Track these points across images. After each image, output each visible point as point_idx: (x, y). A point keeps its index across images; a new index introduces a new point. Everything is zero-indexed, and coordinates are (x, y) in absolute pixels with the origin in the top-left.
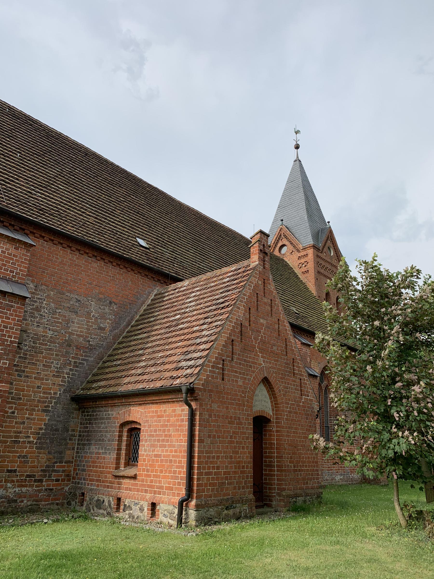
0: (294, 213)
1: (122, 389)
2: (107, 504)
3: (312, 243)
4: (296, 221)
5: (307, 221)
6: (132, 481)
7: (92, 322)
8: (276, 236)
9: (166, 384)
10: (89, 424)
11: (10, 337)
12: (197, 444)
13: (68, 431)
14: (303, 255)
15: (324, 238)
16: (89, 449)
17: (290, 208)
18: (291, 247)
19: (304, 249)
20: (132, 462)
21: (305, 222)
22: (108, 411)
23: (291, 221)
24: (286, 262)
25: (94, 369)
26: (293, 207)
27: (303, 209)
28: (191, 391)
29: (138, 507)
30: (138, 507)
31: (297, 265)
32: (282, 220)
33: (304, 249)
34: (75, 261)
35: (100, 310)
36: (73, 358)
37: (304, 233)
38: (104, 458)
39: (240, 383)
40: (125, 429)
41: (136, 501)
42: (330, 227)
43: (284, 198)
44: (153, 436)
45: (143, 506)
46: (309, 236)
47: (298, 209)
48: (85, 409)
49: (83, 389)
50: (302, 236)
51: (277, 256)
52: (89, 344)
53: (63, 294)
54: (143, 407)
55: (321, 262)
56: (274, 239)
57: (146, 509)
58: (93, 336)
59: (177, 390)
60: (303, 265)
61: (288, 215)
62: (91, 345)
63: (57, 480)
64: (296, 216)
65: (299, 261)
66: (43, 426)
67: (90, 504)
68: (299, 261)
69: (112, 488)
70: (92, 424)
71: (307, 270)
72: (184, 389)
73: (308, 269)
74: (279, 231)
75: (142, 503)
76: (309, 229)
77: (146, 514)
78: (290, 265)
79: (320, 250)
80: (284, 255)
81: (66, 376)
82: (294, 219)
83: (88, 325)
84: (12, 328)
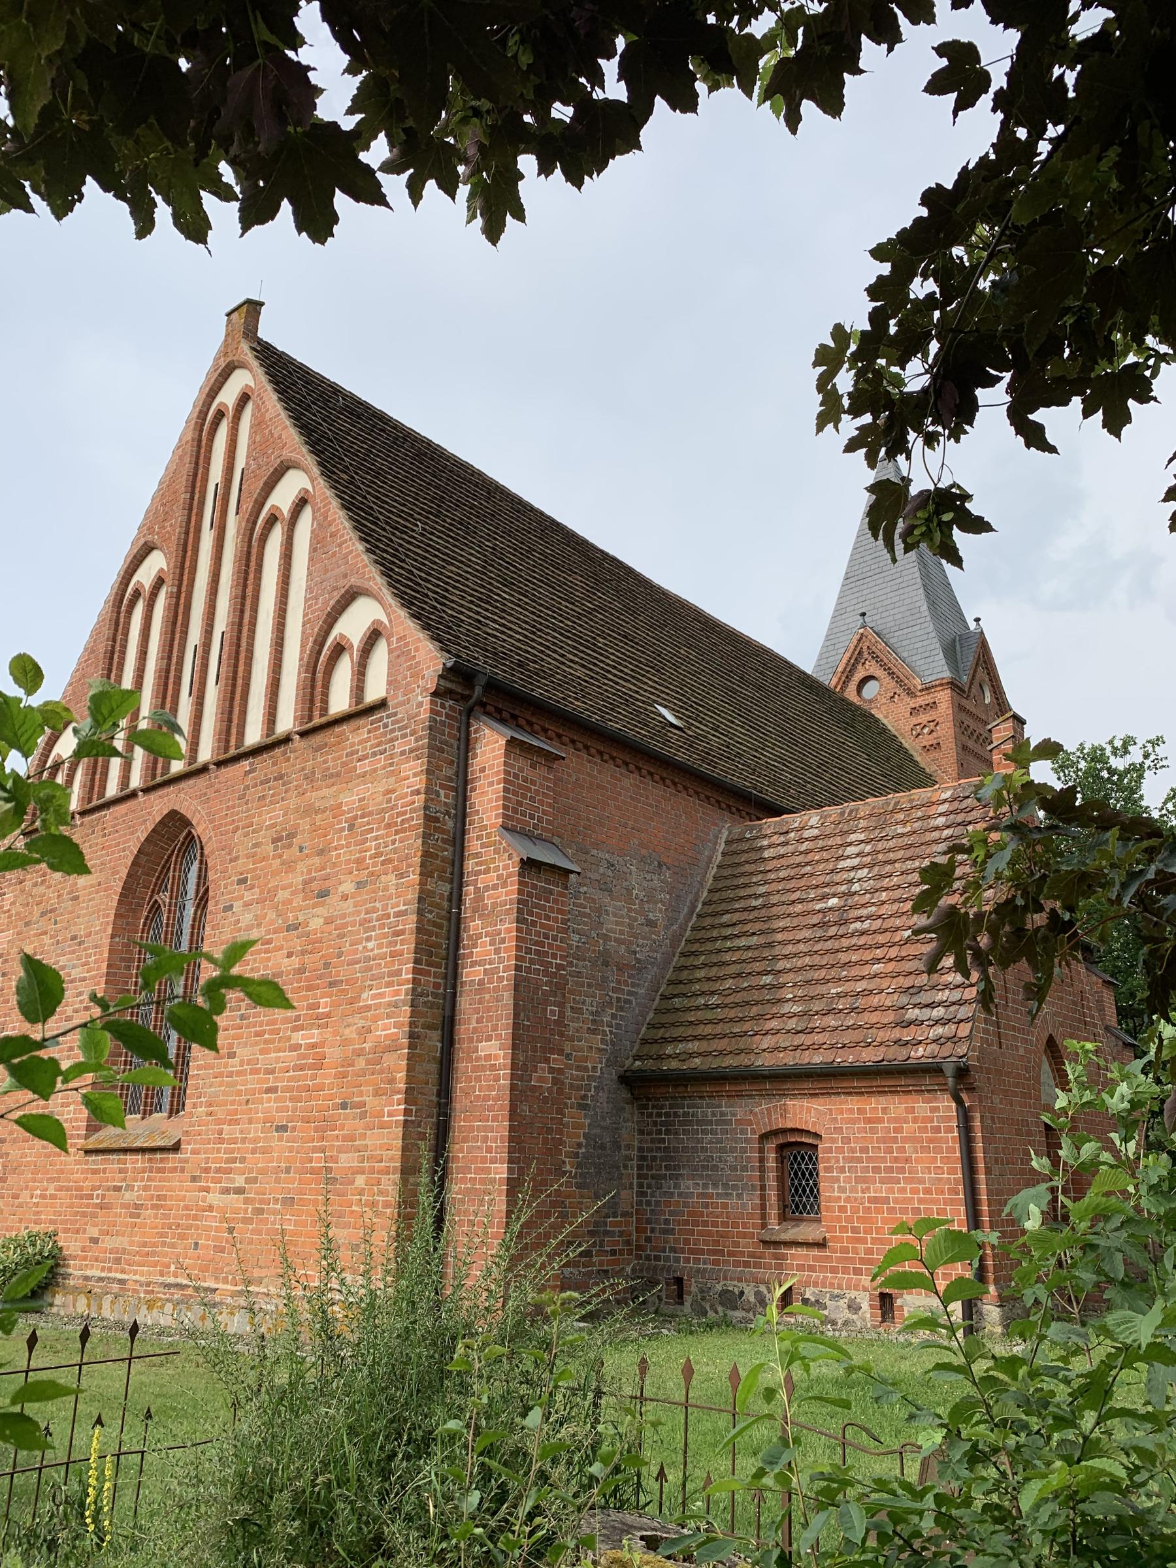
0: (889, 595)
1: (765, 1061)
2: (752, 1299)
3: (947, 674)
4: (897, 617)
5: (928, 618)
6: (815, 1252)
7: (635, 911)
8: (848, 655)
9: (891, 1057)
10: (668, 1132)
11: (554, 956)
12: (982, 1177)
13: (619, 1148)
14: (923, 703)
15: (969, 660)
16: (676, 1186)
17: (879, 582)
18: (891, 684)
19: (927, 689)
20: (793, 1212)
21: (922, 620)
22: (720, 1106)
23: (884, 615)
24: (877, 721)
25: (647, 1013)
26: (887, 579)
27: (915, 587)
28: (962, 1073)
29: (843, 1303)
30: (843, 1303)
31: (908, 728)
32: (863, 614)
33: (927, 689)
34: (595, 777)
35: (645, 884)
36: (615, 990)
37: (923, 650)
38: (725, 1206)
39: (1021, 1052)
40: (771, 1145)
41: (836, 1291)
42: (982, 633)
43: (859, 556)
44: (860, 1160)
45: (858, 1300)
46: (937, 658)
47: (902, 585)
48: (649, 1099)
49: (637, 1057)
50: (918, 657)
51: (851, 704)
52: (636, 959)
53: (587, 853)
54: (821, 1100)
55: (969, 721)
56: (845, 661)
57: (865, 1306)
58: (641, 942)
59: (932, 1070)
60: (926, 730)
61: (873, 601)
62: (638, 961)
63: (613, 1253)
64: (897, 605)
65: (915, 720)
66: (582, 1140)
67: (703, 1299)
68: (915, 720)
69: (757, 1265)
70: (677, 1133)
71: (935, 742)
72: (949, 1070)
73: (940, 740)
74: (856, 642)
75: (853, 1294)
76: (936, 640)
77: (869, 1316)
78: (890, 727)
79: (964, 692)
80: (871, 701)
81: (607, 1029)
82: (892, 612)
83: (630, 917)
84: (555, 939)
